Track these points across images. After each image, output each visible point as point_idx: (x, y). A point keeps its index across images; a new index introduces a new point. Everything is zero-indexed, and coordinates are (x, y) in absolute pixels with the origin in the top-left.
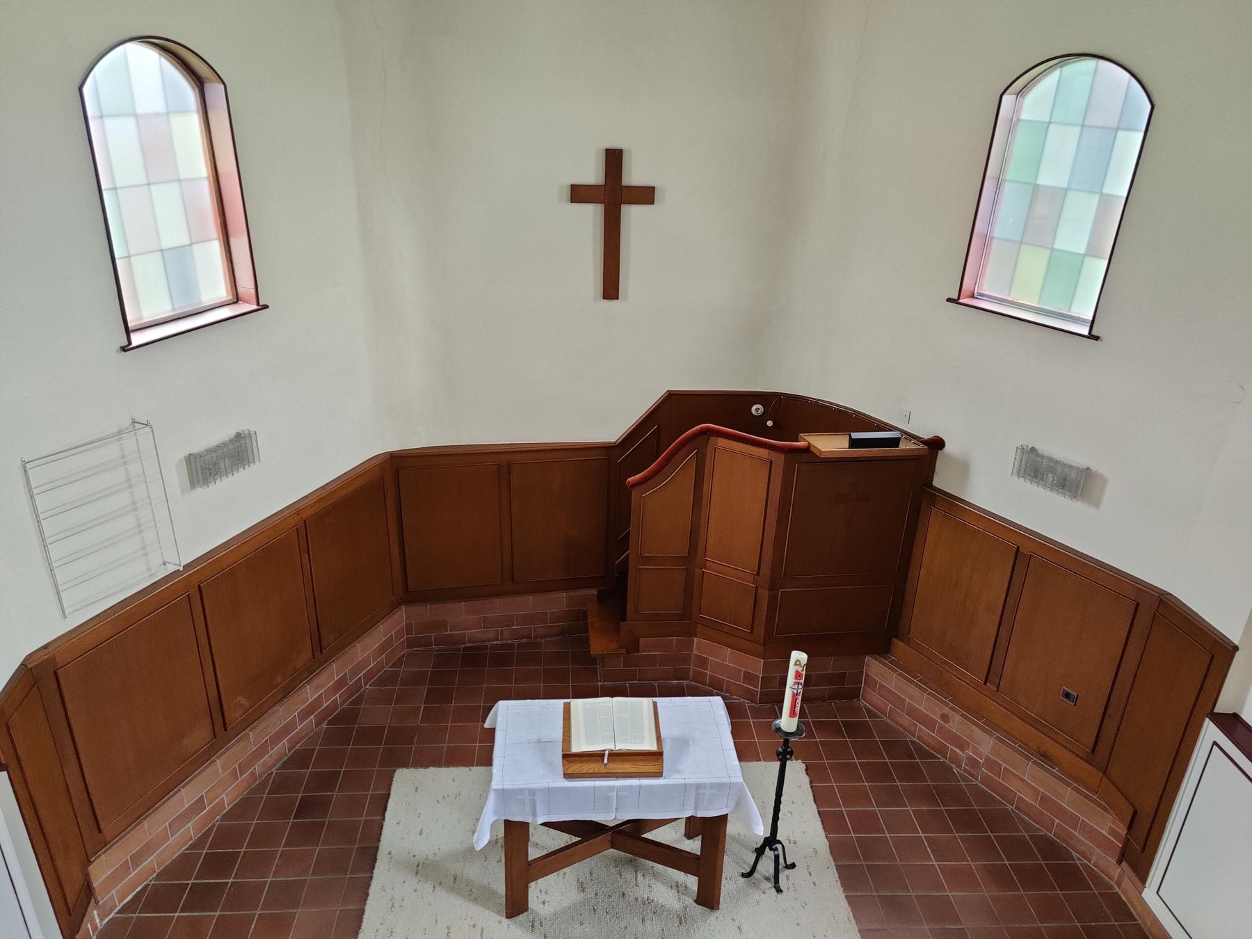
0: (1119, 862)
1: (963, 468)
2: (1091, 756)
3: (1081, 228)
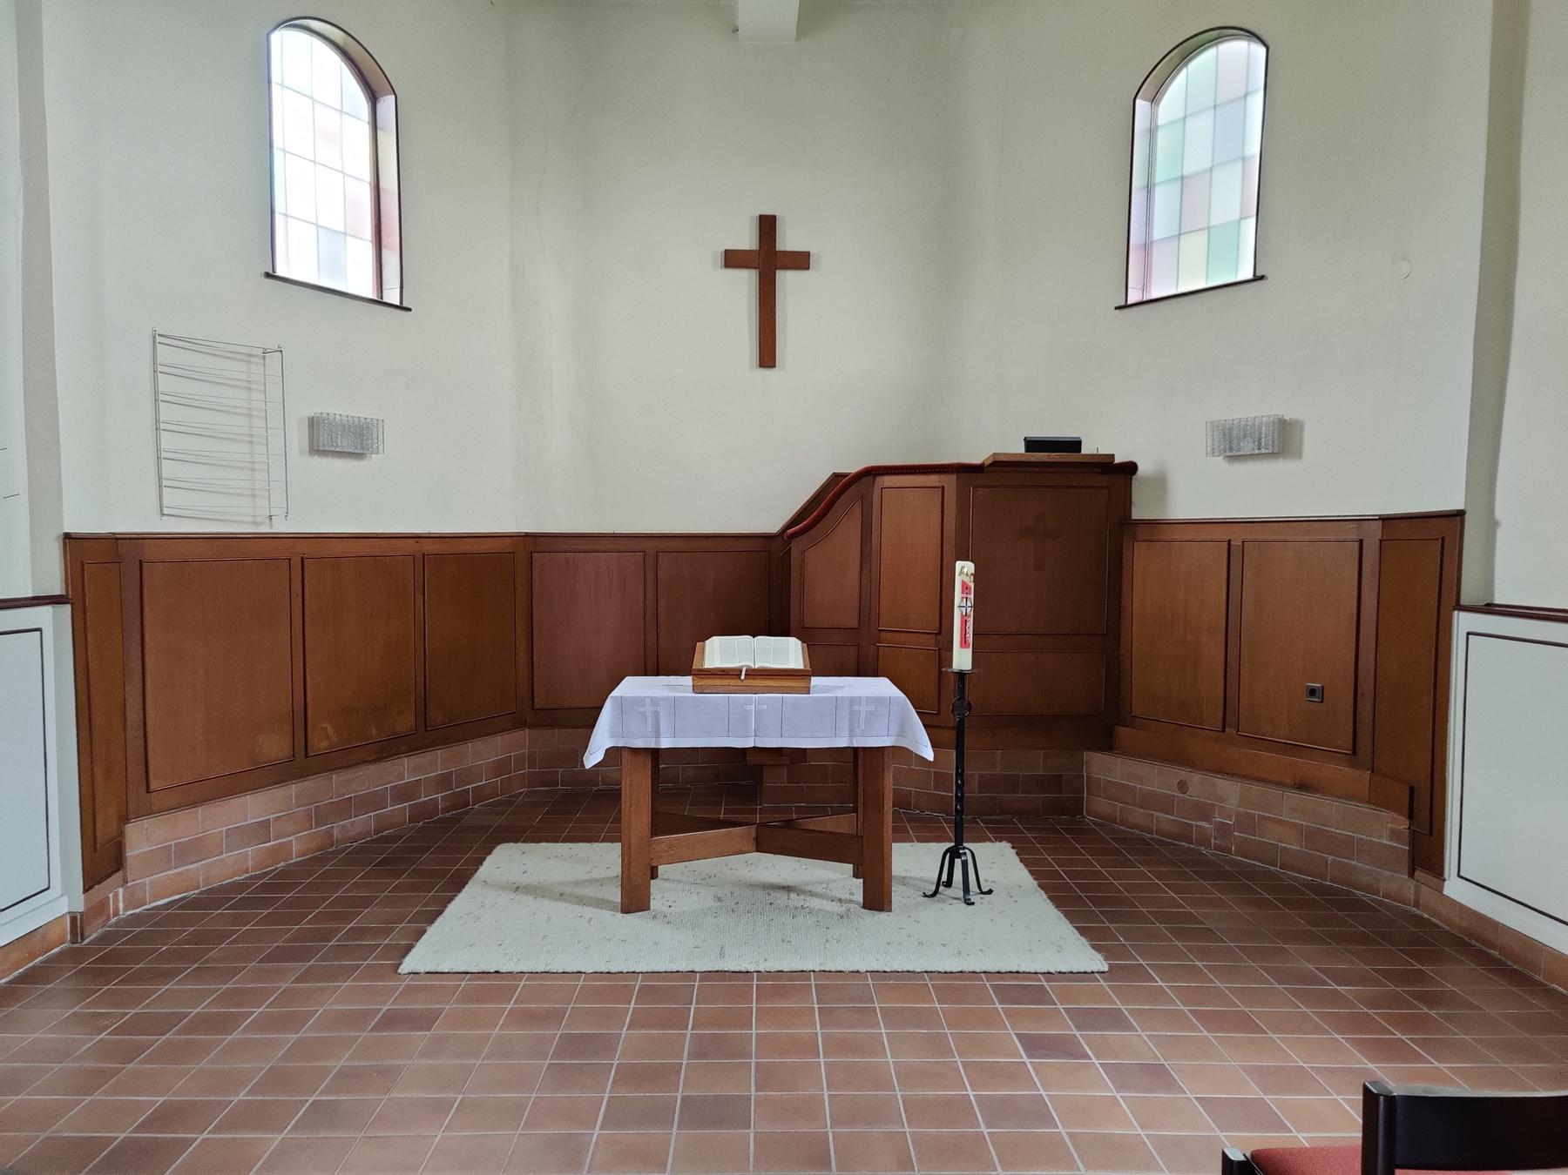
0: (1411, 874)
1: (1160, 482)
2: (1353, 755)
3: (1233, 196)
